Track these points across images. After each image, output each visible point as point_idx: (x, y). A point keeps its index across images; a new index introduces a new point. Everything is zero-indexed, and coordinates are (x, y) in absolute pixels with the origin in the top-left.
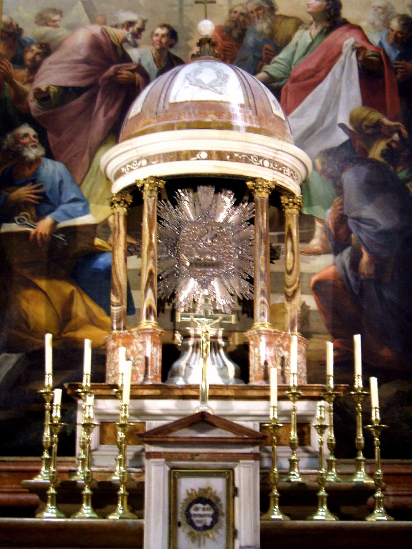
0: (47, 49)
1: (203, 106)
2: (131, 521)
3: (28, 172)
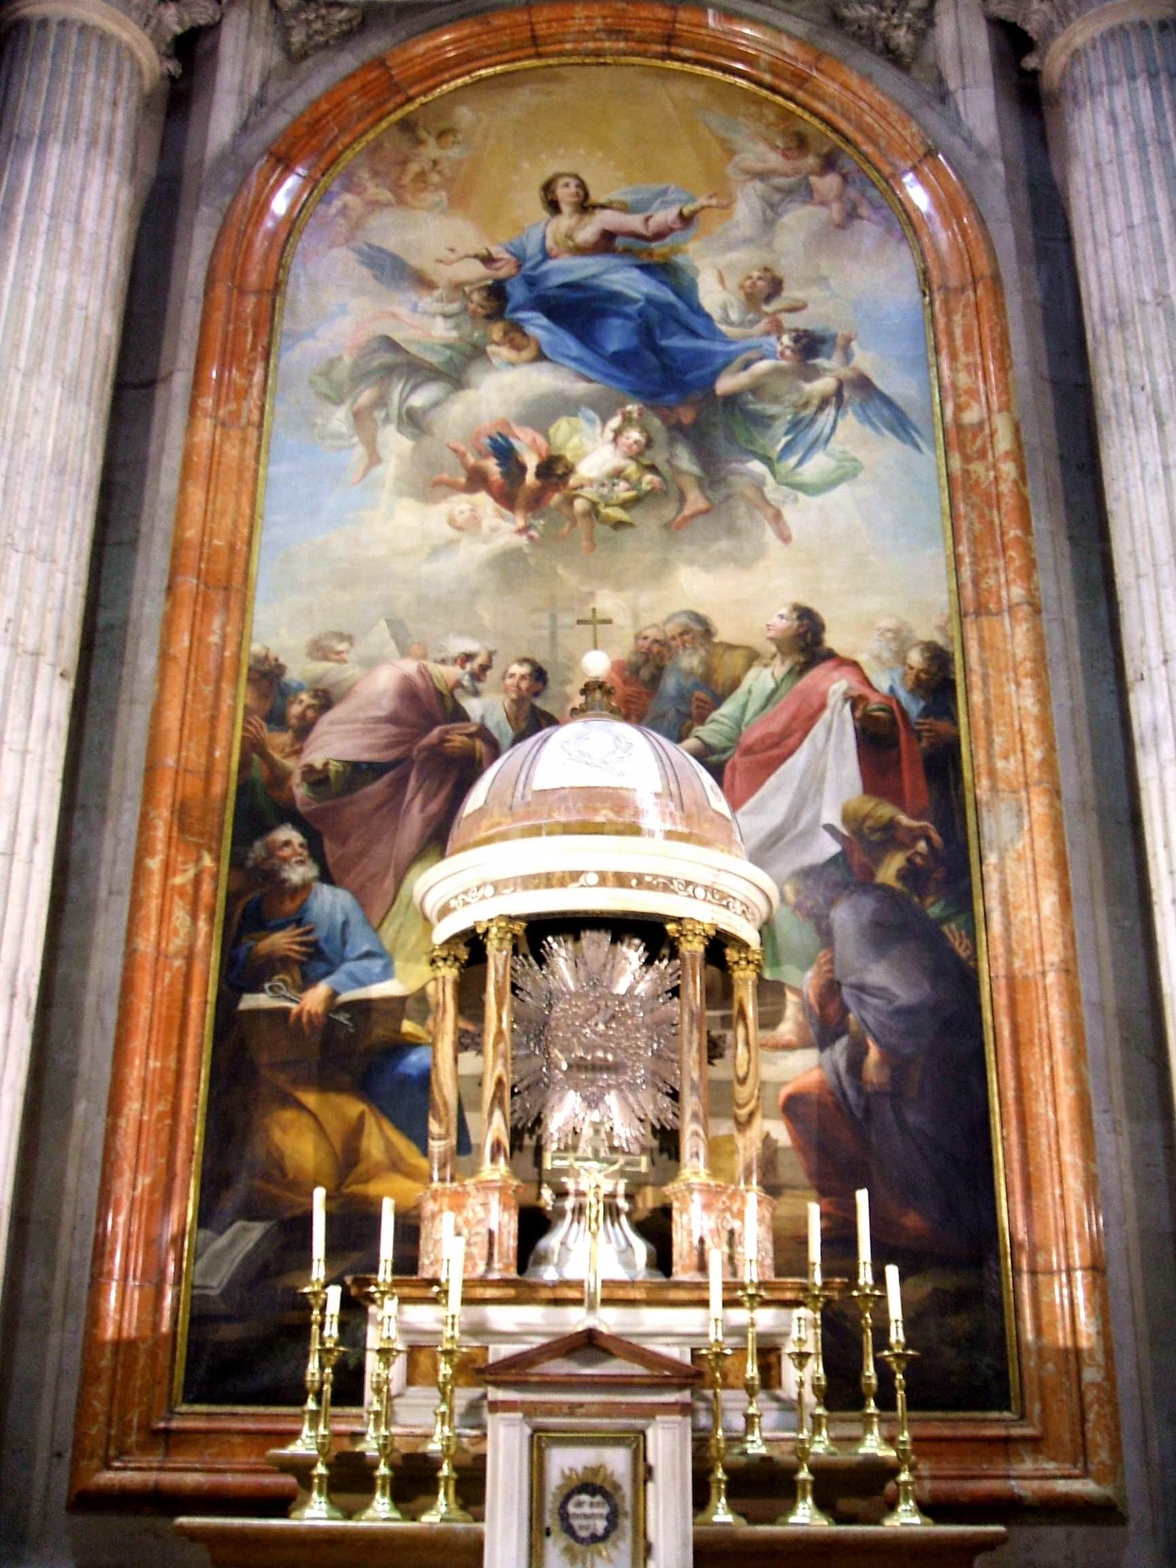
0: (325, 700)
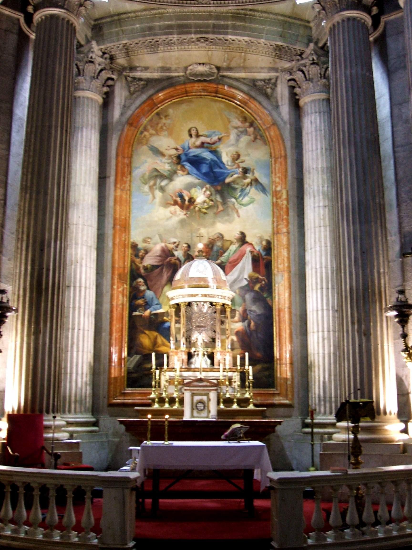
0: (146, 252)
1: (200, 279)
2: (180, 408)
3: (141, 295)
